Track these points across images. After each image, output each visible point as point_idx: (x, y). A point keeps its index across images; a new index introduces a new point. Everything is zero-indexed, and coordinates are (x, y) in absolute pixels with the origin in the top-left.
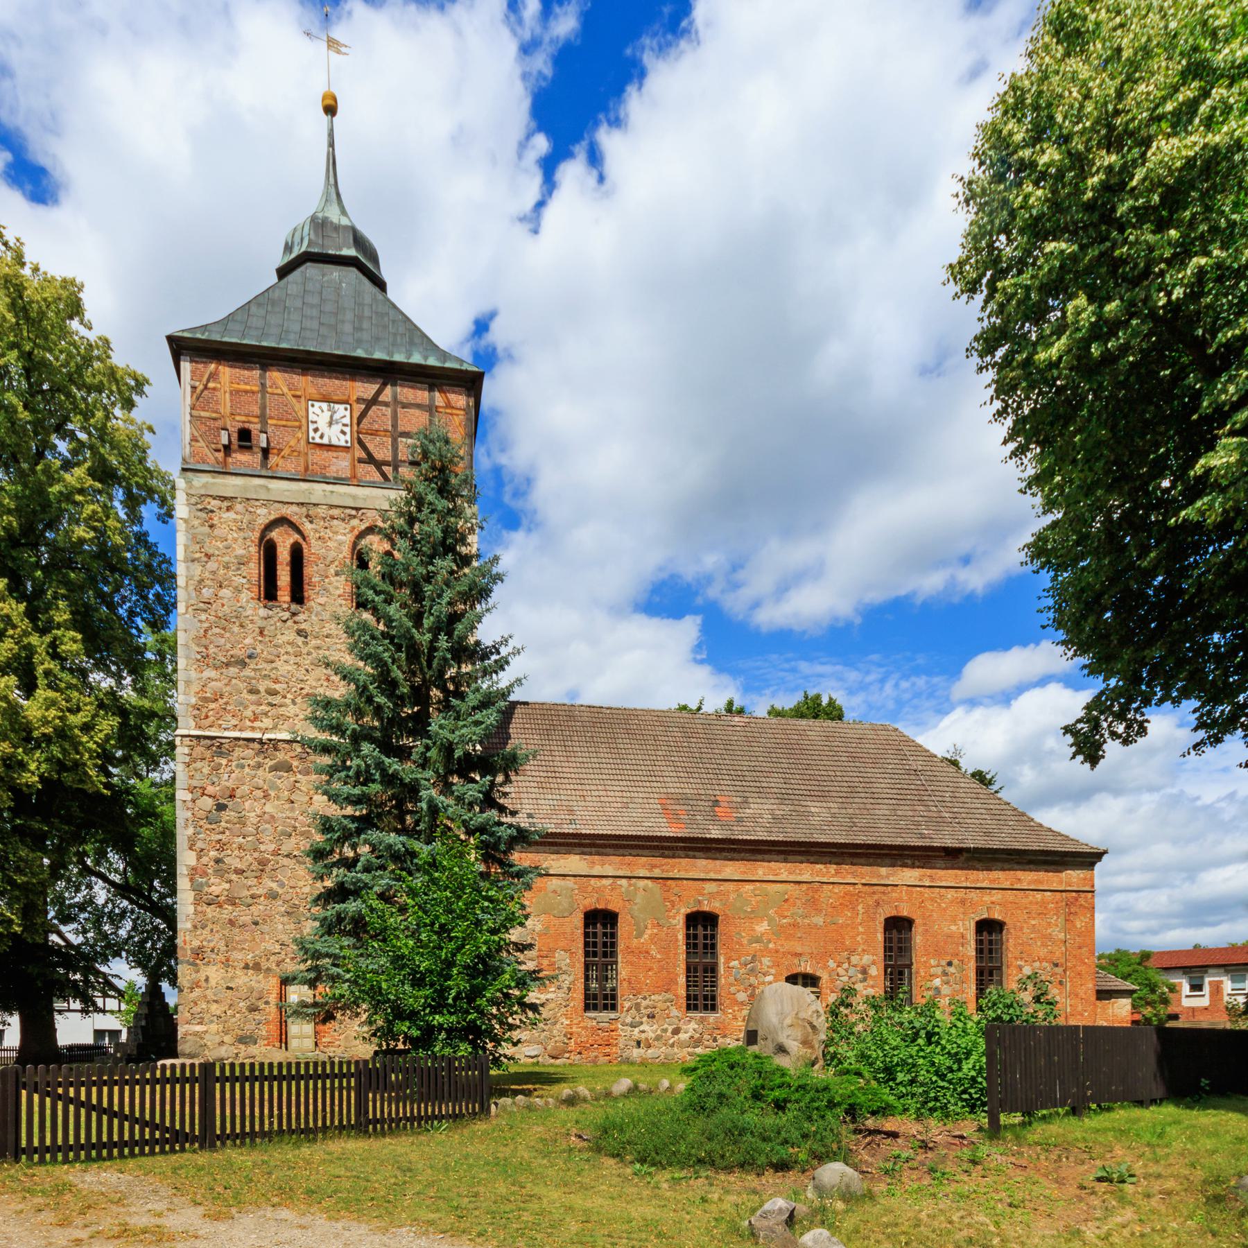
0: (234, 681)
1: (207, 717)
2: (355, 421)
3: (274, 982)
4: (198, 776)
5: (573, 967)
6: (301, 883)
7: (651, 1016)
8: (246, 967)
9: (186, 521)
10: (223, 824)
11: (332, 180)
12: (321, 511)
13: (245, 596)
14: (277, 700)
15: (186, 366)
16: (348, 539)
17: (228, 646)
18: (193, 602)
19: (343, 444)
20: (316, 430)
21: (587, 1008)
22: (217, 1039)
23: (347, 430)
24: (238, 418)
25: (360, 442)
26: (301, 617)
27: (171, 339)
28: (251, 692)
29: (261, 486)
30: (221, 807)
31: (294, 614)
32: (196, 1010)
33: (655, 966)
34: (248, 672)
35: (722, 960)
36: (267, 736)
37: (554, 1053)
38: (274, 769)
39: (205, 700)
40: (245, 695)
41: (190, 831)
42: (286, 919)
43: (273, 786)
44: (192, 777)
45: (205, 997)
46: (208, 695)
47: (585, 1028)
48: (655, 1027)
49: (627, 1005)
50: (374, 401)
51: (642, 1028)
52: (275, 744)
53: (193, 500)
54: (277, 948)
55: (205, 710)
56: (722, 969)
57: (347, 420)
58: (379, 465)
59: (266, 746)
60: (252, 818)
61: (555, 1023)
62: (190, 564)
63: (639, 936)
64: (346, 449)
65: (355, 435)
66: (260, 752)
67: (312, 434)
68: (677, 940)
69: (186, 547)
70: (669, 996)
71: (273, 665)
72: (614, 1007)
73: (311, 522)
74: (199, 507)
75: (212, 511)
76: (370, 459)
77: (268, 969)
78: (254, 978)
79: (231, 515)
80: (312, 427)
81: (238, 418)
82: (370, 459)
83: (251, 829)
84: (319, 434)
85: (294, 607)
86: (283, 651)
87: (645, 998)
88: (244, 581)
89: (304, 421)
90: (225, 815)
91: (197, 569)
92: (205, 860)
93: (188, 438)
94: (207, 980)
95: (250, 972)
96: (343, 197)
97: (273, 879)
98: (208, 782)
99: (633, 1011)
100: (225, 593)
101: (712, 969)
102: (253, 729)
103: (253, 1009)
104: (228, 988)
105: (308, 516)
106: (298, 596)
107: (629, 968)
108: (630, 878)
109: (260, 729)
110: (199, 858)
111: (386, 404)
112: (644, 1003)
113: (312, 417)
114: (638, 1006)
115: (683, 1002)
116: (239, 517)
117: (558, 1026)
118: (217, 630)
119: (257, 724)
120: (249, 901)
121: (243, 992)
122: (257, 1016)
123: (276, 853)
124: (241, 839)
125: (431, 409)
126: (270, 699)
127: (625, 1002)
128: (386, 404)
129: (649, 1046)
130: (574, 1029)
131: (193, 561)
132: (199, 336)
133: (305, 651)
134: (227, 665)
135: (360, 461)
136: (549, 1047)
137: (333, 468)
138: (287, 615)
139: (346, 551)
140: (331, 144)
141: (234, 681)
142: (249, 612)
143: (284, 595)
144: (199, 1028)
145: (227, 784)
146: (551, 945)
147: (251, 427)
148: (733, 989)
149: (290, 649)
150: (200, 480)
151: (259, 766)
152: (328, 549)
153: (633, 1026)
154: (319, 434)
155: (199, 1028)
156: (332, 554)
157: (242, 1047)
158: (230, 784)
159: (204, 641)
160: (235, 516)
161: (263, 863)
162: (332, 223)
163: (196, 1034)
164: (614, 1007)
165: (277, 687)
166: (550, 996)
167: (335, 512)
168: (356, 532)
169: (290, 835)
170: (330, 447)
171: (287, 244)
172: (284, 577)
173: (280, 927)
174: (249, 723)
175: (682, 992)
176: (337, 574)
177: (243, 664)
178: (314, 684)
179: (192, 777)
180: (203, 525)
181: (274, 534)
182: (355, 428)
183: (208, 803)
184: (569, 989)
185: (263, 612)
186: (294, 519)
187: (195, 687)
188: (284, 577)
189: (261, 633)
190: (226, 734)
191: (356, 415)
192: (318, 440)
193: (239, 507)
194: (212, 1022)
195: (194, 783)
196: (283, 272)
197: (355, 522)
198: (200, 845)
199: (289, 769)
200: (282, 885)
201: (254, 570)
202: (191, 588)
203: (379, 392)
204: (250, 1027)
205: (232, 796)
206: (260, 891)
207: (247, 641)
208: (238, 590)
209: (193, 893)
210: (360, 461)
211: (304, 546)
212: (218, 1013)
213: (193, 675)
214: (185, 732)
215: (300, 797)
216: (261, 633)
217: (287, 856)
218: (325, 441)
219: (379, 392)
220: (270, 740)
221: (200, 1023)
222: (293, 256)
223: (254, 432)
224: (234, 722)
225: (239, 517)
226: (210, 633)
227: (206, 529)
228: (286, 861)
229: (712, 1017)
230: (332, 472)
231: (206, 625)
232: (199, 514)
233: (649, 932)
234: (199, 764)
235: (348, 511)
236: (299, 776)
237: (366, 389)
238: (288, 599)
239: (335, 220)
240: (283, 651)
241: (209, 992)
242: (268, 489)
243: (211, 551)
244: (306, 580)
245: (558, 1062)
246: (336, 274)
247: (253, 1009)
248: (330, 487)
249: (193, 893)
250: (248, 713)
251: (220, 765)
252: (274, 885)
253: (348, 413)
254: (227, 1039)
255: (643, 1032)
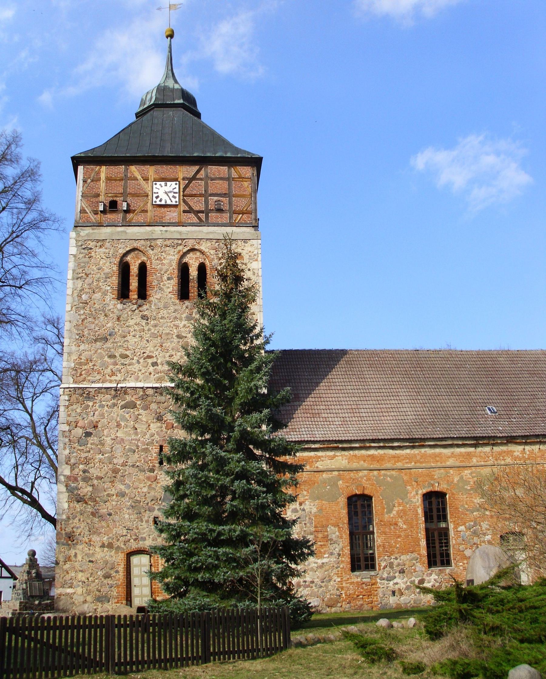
0: (99, 351)
1: (81, 375)
2: (182, 190)
3: (121, 557)
4: (73, 414)
5: (341, 538)
6: (142, 485)
7: (402, 572)
8: (103, 546)
9: (75, 256)
10: (89, 445)
11: (170, 68)
12: (159, 242)
13: (109, 297)
14: (127, 361)
15: (80, 168)
16: (176, 257)
17: (97, 328)
18: (75, 303)
19: (174, 203)
20: (157, 197)
21: (353, 569)
22: (82, 599)
23: (177, 195)
24: (110, 195)
25: (184, 201)
26: (145, 307)
27: (73, 158)
28: (110, 357)
29: (122, 232)
30: (88, 434)
31: (140, 306)
32: (68, 577)
33: (402, 534)
34: (109, 345)
35: (451, 526)
36: (119, 385)
37: (329, 604)
38: (123, 407)
39: (81, 364)
40: (106, 358)
41: (67, 452)
42: (130, 511)
43: (123, 418)
44: (69, 416)
45: (74, 568)
46: (82, 361)
47: (352, 583)
48: (405, 579)
49: (383, 564)
50: (194, 178)
51: (395, 581)
52: (125, 390)
53: (80, 244)
54: (125, 532)
55: (79, 371)
56: (452, 533)
57: (177, 190)
58: (196, 213)
59: (119, 392)
60: (108, 441)
61: (330, 580)
62: (75, 281)
63: (390, 511)
64: (175, 206)
65: (182, 198)
66: (114, 397)
67: (154, 199)
68: (417, 514)
69: (74, 271)
70: (415, 555)
71: (126, 339)
72: (373, 567)
73: (153, 250)
74: (83, 247)
75: (91, 249)
76: (190, 210)
77: (118, 548)
78: (108, 554)
79: (103, 250)
80: (155, 195)
81: (110, 195)
82: (190, 210)
83: (108, 448)
84: (159, 199)
85: (140, 301)
86: (132, 330)
87: (396, 559)
88: (109, 288)
89: (150, 193)
90: (90, 440)
91: (79, 283)
92: (77, 470)
93: (79, 210)
94: (76, 555)
95: (106, 549)
96: (175, 74)
97: (122, 482)
98: (80, 418)
99: (388, 569)
100: (98, 296)
101: (445, 533)
102: (111, 382)
103: (107, 576)
104: (90, 561)
105: (150, 246)
106: (143, 294)
107: (383, 537)
108: (379, 470)
109: (116, 380)
110: (72, 469)
111: (201, 179)
112: (396, 562)
113: (155, 190)
114: (391, 565)
115: (425, 559)
116: (107, 251)
117: (332, 583)
118: (90, 320)
119: (113, 378)
120: (105, 498)
121: (101, 564)
122: (109, 581)
123: (124, 464)
124: (100, 456)
125: (228, 179)
126: (123, 361)
127: (381, 562)
128: (201, 179)
129: (402, 594)
130: (344, 585)
131: (77, 279)
132: (90, 155)
133: (146, 328)
134: (96, 341)
135: (184, 212)
136: (326, 599)
137: (168, 218)
138: (135, 307)
139: (175, 265)
140: (170, 52)
141: (99, 351)
142: (111, 307)
143: (134, 295)
144: (70, 591)
145: (92, 418)
146: (324, 523)
147: (117, 199)
148: (461, 547)
149: (136, 328)
150: (85, 232)
151: (114, 405)
152: (163, 264)
153: (389, 579)
154: (159, 199)
155: (70, 591)
156: (165, 268)
157: (100, 605)
158: (95, 419)
159: (81, 328)
160: (105, 250)
161: (115, 471)
162: (169, 88)
163: (67, 594)
164: (373, 567)
165: (128, 353)
166: (325, 560)
167: (168, 243)
168: (181, 253)
169: (135, 451)
170: (166, 206)
171: (142, 99)
172: (134, 284)
173: (127, 516)
174: (108, 378)
175: (424, 552)
176: (169, 279)
177: (106, 339)
178: (152, 349)
179: (69, 416)
180: (85, 257)
181: (129, 258)
182: (182, 193)
183: (79, 432)
184: (339, 555)
185: (120, 306)
186: (142, 248)
187: (74, 357)
188: (134, 284)
189: (118, 319)
190: (93, 385)
191: (182, 187)
192: (158, 203)
193: (107, 245)
194: (79, 586)
195: (70, 419)
196: (139, 115)
197: (180, 248)
198: (73, 461)
199: (134, 406)
200: (128, 487)
201: (115, 280)
202: (75, 295)
203: (198, 172)
204: (105, 590)
205: (95, 427)
206: (113, 492)
207: (109, 325)
208: (105, 293)
209: (67, 494)
210: (184, 212)
211: (148, 264)
212: (84, 579)
213: (74, 348)
214: (67, 386)
215: (141, 428)
216: (118, 319)
217: (133, 466)
218: (163, 203)
219: (198, 172)
220: (122, 388)
221: (71, 587)
222: (146, 106)
223: (119, 202)
224: (98, 377)
225: (107, 251)
226: (85, 321)
227: (87, 259)
228: (131, 470)
229: (448, 570)
230: (167, 219)
231: (83, 317)
232: (83, 251)
233: (396, 509)
234: (74, 407)
235: (176, 241)
236: (141, 411)
237: (190, 170)
238: (136, 297)
239: (171, 86)
240: (132, 330)
241: (77, 565)
242: (125, 232)
243: (88, 272)
244: (148, 284)
245: (333, 610)
246: (171, 113)
247: (107, 576)
248: (165, 228)
249: (67, 494)
250: (108, 371)
251: (88, 406)
252: (122, 487)
253: (177, 186)
254: (89, 598)
255: (397, 584)
